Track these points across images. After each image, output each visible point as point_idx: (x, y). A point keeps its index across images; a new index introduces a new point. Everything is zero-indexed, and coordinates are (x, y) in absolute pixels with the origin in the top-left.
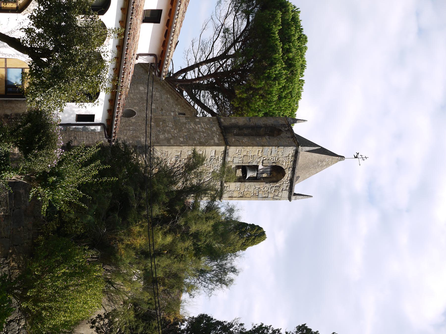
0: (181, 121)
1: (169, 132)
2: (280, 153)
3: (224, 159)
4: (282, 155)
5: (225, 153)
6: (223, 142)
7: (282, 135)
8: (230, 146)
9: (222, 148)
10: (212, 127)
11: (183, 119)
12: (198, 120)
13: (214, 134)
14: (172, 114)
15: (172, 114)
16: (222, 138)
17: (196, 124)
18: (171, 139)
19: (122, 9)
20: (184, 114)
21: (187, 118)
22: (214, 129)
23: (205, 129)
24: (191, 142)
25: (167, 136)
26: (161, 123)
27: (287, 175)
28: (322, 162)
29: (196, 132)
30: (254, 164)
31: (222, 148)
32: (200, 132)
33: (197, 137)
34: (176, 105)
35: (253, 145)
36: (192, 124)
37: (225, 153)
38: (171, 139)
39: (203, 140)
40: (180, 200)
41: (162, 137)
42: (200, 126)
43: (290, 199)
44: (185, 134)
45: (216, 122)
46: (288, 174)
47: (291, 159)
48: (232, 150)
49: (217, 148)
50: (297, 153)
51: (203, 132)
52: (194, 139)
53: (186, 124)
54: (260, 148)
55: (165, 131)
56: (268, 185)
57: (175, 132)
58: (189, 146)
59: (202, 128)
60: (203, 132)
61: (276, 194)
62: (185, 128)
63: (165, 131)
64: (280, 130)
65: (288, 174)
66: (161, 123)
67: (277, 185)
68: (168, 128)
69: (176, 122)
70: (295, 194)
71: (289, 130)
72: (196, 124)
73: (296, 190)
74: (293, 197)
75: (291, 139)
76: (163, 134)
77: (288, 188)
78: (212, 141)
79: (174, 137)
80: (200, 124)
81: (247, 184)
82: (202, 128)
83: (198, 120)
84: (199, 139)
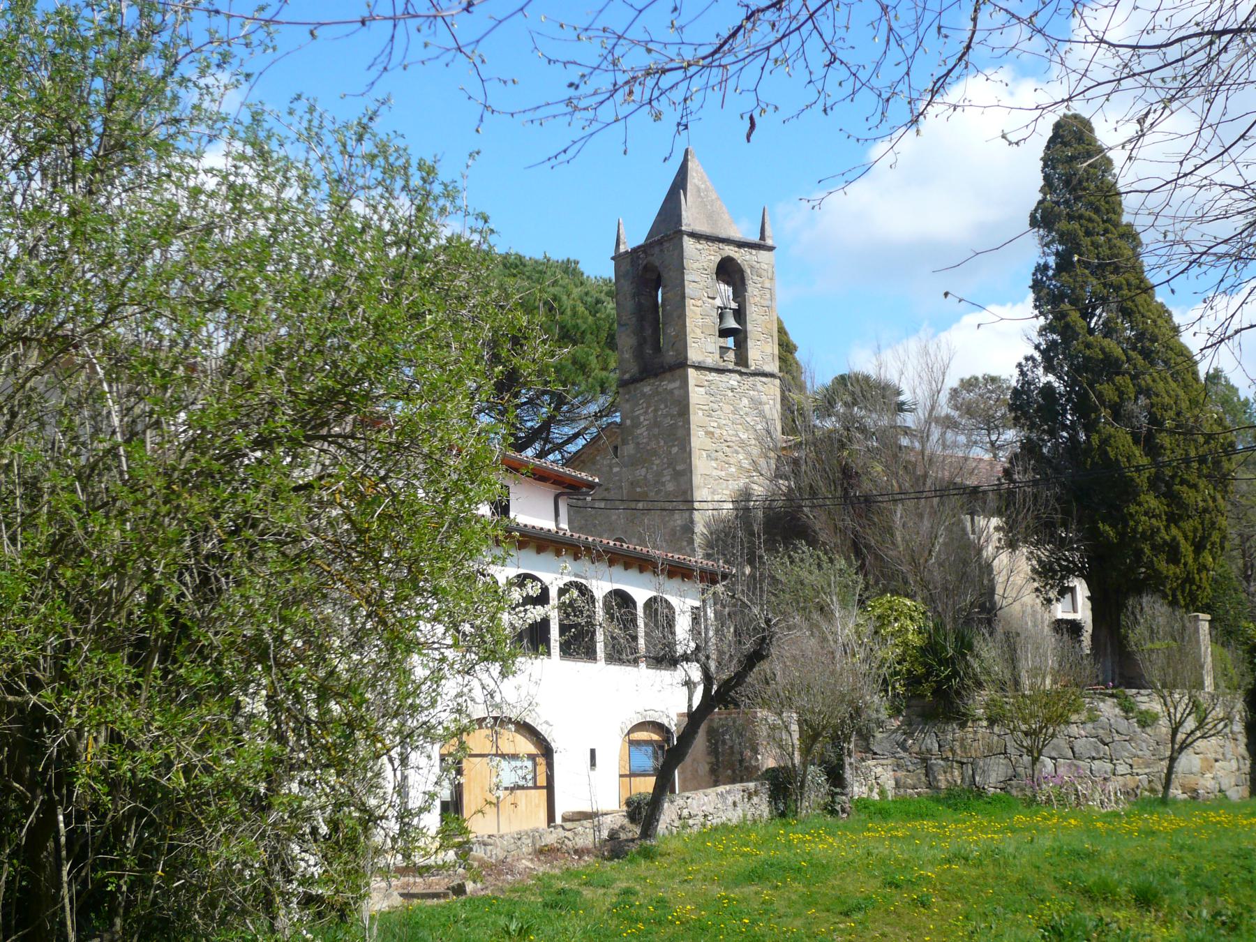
0: (632, 452)
1: (659, 474)
2: (696, 265)
3: (710, 370)
4: (699, 261)
5: (699, 368)
6: (678, 372)
7: (657, 264)
8: (686, 358)
9: (691, 371)
10: (644, 395)
11: (628, 450)
12: (628, 422)
13: (660, 389)
14: (616, 470)
15: (616, 470)
16: (668, 375)
17: (636, 425)
18: (674, 469)
19: (626, 569)
20: (616, 448)
21: (624, 442)
22: (647, 389)
23: (647, 408)
24: (680, 433)
25: (668, 478)
26: (638, 490)
27: (732, 254)
28: (699, 190)
29: (656, 424)
30: (715, 313)
31: (691, 371)
32: (655, 417)
33: (668, 421)
34: (594, 464)
35: (682, 316)
36: (639, 432)
37: (699, 368)
38: (674, 469)
39: (675, 411)
40: (1016, 419)
41: (670, 487)
42: (642, 418)
43: (771, 249)
44: (662, 443)
45: (632, 387)
46: (730, 251)
47: (703, 245)
48: (694, 355)
49: (691, 382)
50: (693, 235)
51: (656, 410)
52: (673, 427)
53: (638, 444)
54: (689, 302)
55: (657, 482)
56: (749, 289)
57: (657, 462)
58: (689, 435)
59: (646, 413)
60: (656, 410)
61: (764, 273)
62: (648, 444)
63: (657, 482)
64: (645, 268)
65: (730, 251)
66: (638, 490)
67: (748, 271)
68: (649, 476)
69: (634, 462)
70: (763, 237)
71: (645, 252)
72: (636, 425)
73: (754, 238)
74: (769, 242)
75: (666, 245)
76: (663, 484)
77: (754, 252)
78: (676, 392)
79: (671, 464)
80: (638, 417)
81: (749, 327)
82: (646, 413)
83: (628, 422)
84: (672, 416)
